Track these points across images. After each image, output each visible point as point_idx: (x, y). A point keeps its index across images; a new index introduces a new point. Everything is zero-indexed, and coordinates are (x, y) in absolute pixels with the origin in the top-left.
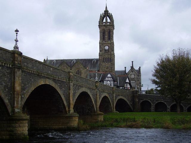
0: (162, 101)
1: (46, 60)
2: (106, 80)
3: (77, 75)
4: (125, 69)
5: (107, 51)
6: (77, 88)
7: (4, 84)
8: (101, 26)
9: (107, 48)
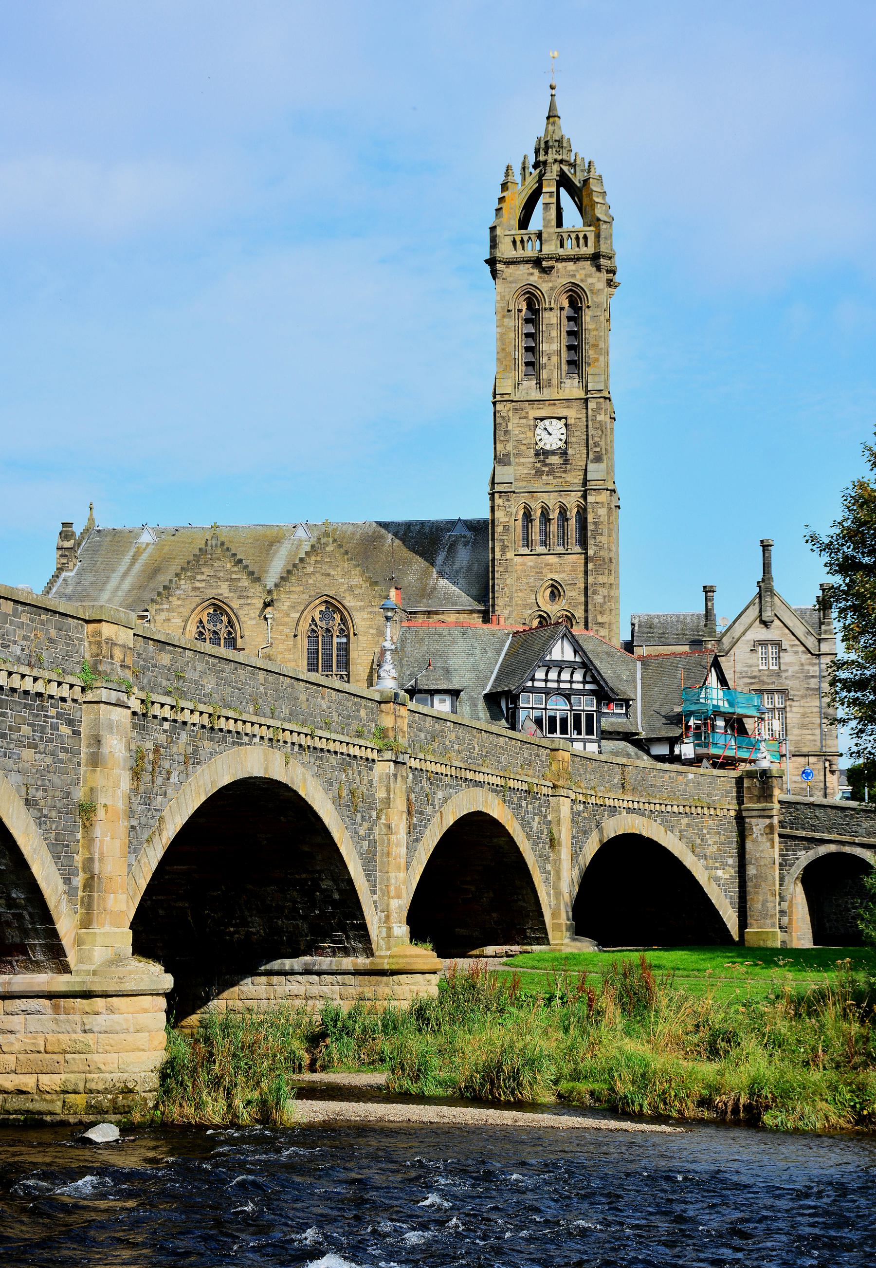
1: (78, 530)
2: (533, 690)
3: (207, 647)
5: (555, 460)
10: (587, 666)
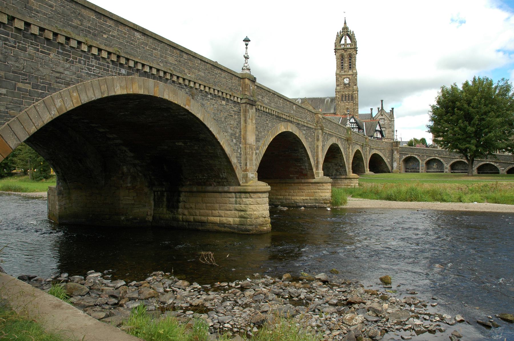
0: (436, 158)
4: (371, 111)
5: (347, 85)
6: (326, 138)
7: (229, 130)
8: (338, 50)
9: (346, 81)
10: (356, 123)
